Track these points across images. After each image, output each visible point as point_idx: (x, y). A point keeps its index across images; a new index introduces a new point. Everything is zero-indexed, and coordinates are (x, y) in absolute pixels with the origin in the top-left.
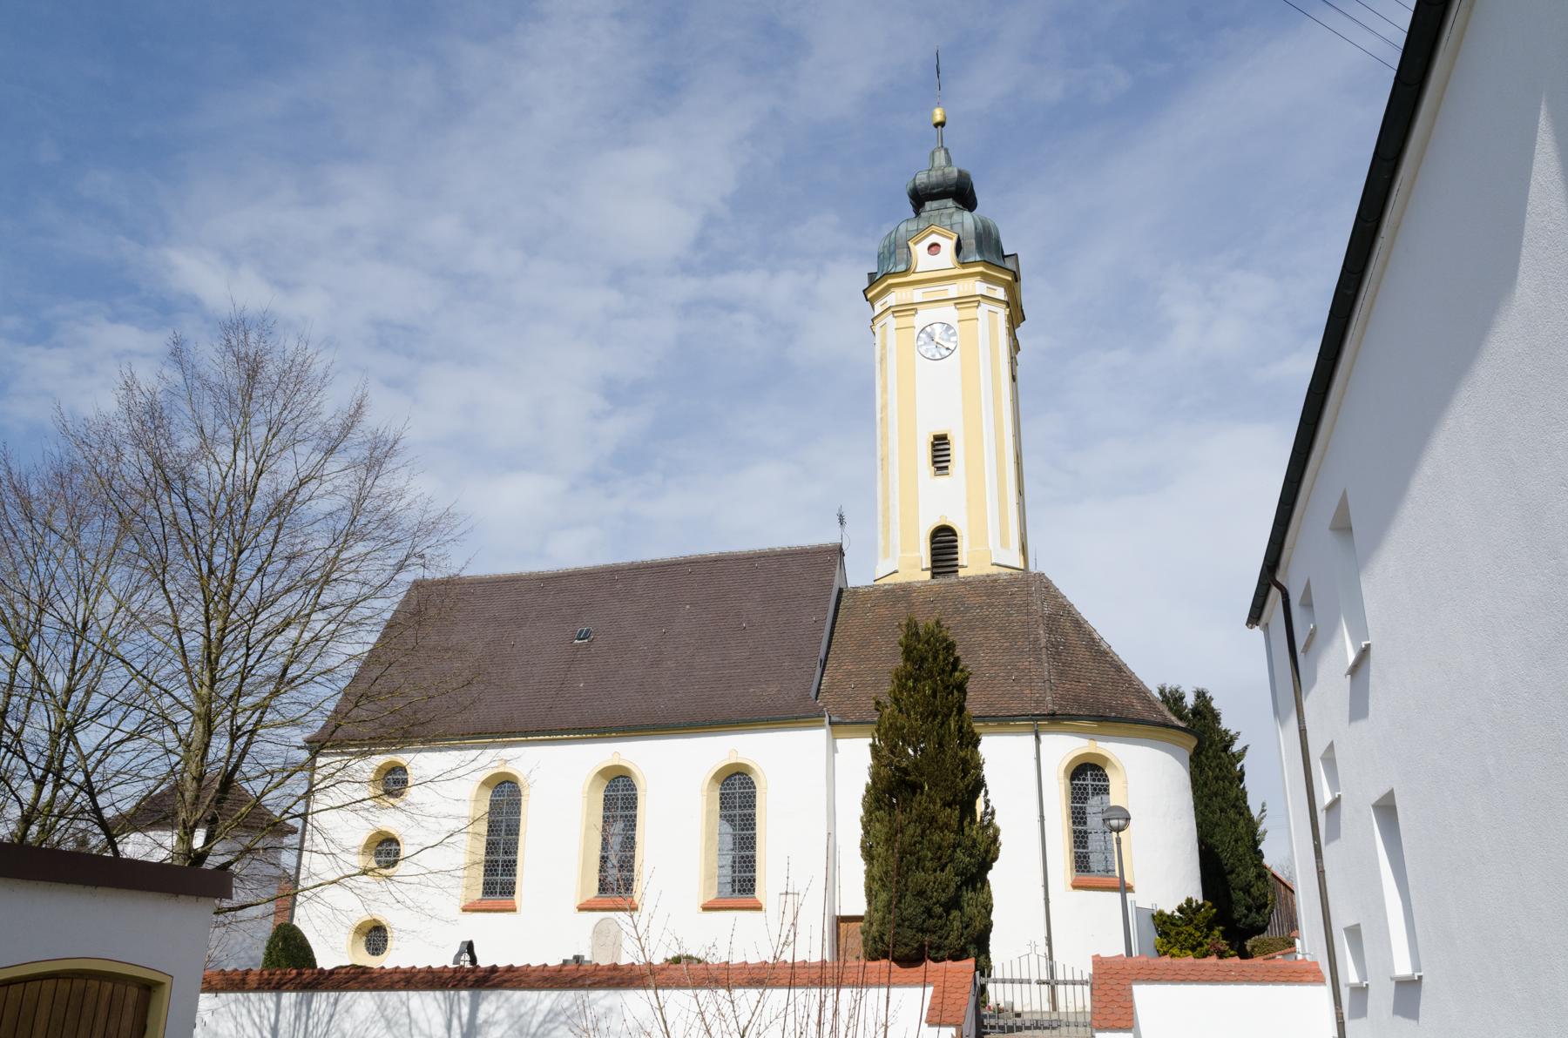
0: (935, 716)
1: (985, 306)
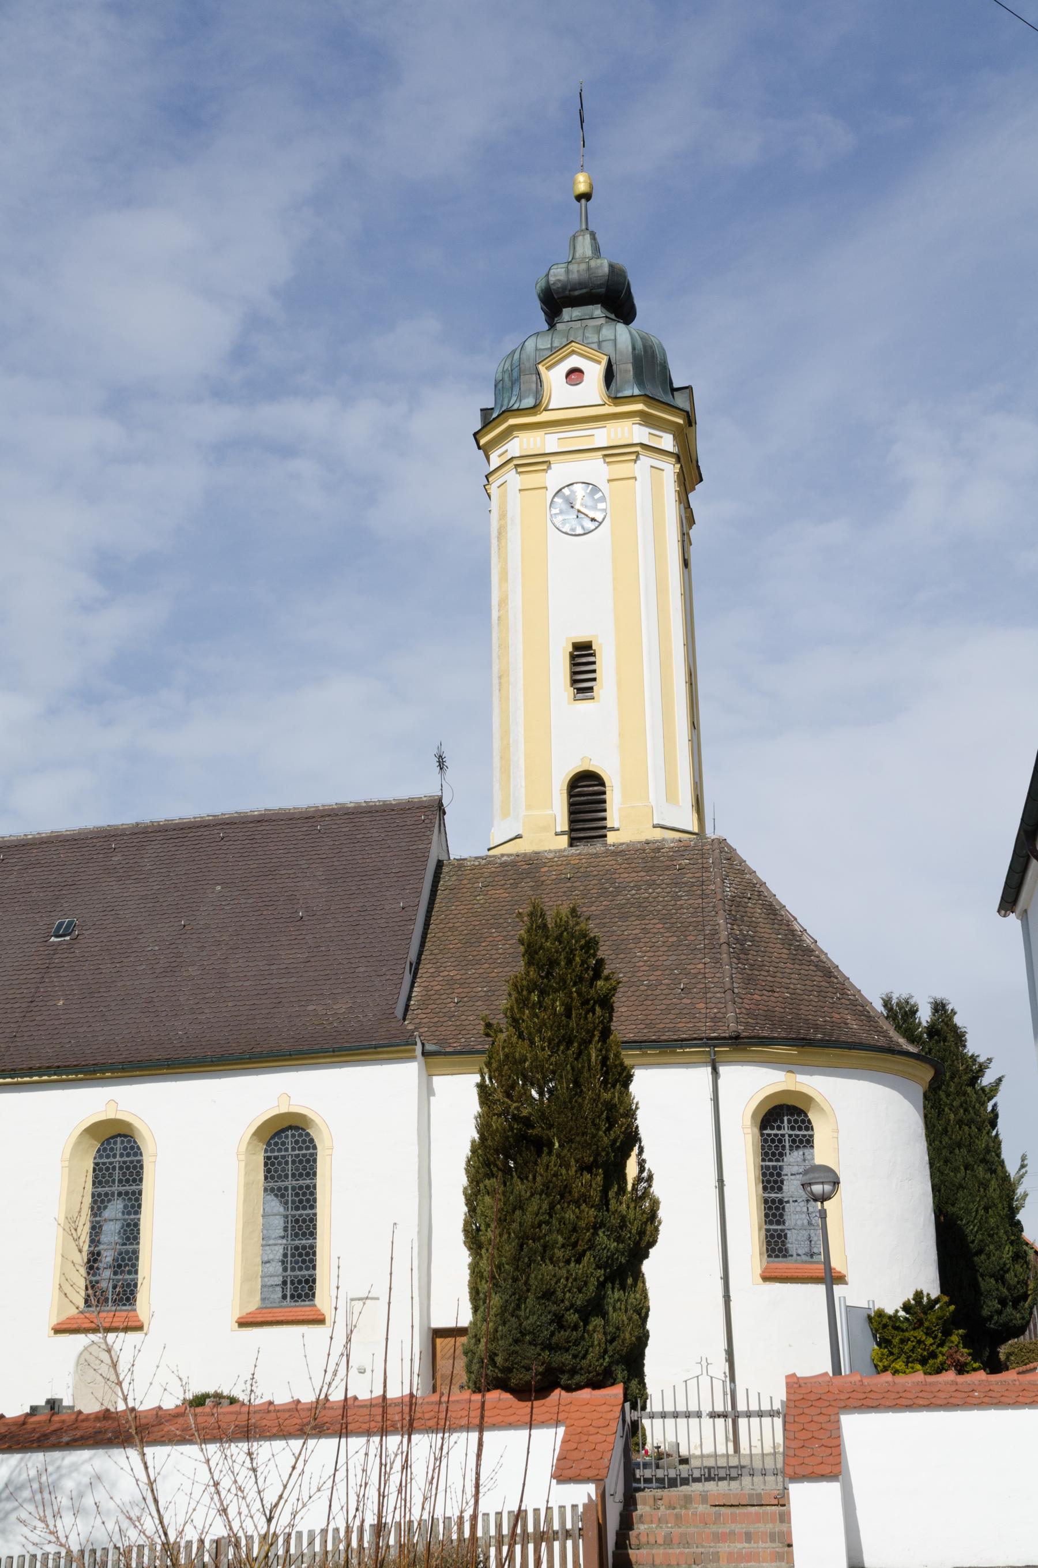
0: (569, 1044)
1: (647, 460)
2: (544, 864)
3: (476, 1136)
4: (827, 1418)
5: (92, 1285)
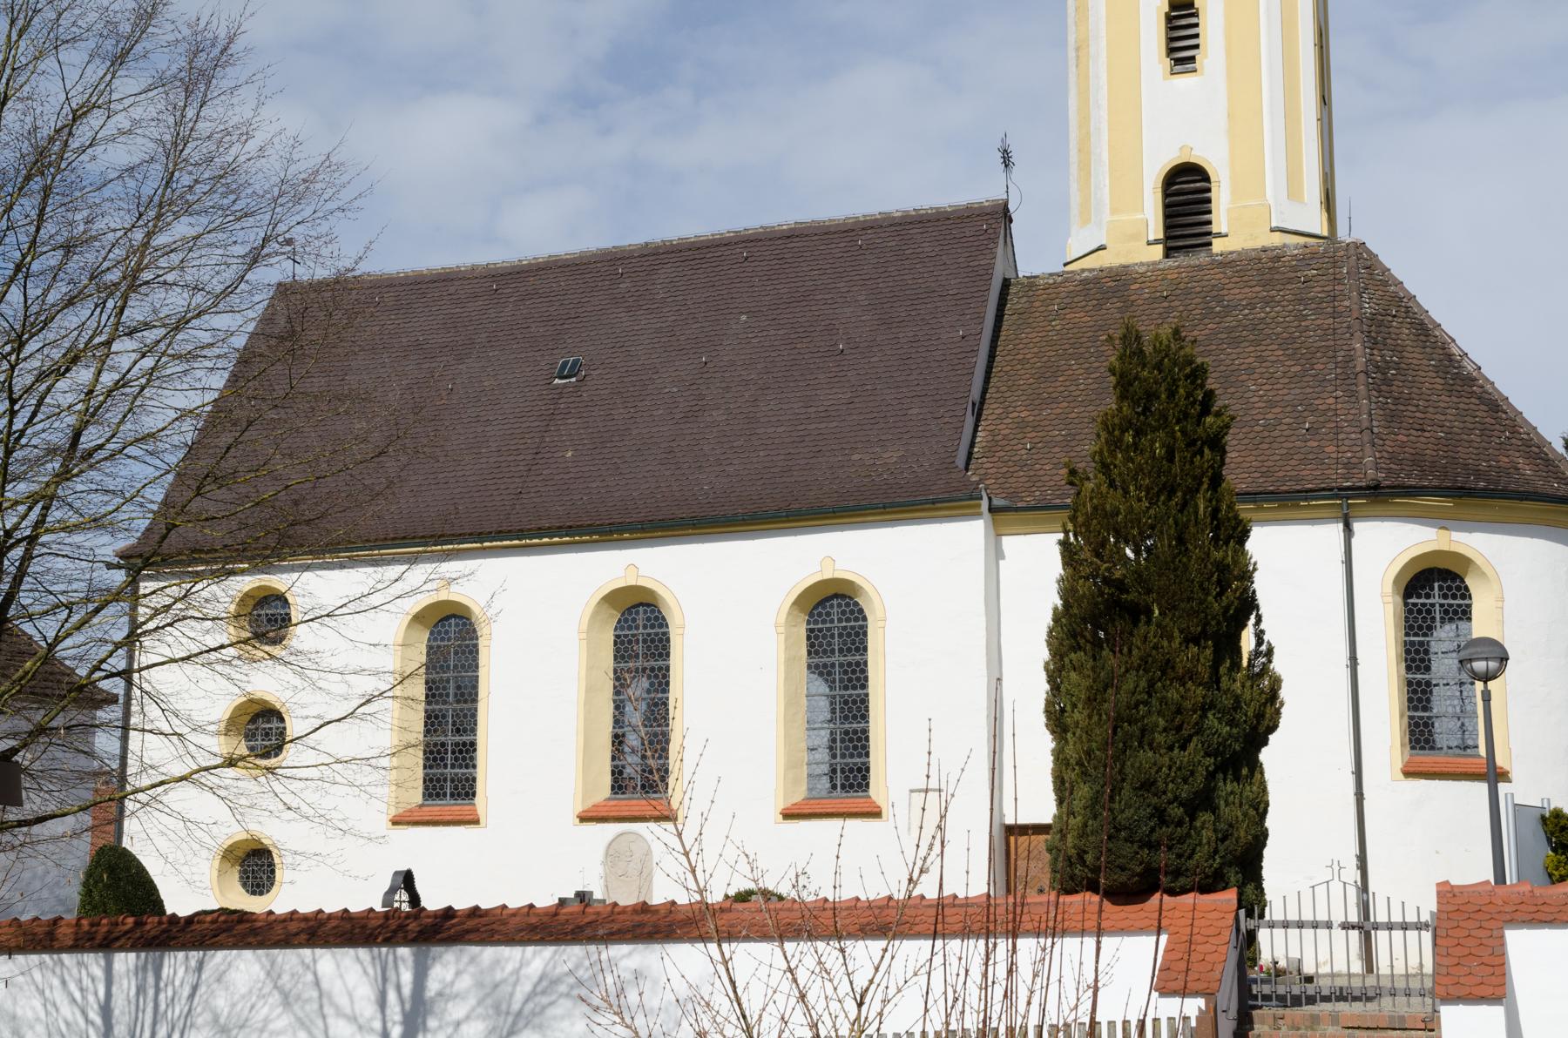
0: (1171, 493)
2: (1135, 281)
3: (1059, 603)
4: (1488, 933)
5: (617, 773)
